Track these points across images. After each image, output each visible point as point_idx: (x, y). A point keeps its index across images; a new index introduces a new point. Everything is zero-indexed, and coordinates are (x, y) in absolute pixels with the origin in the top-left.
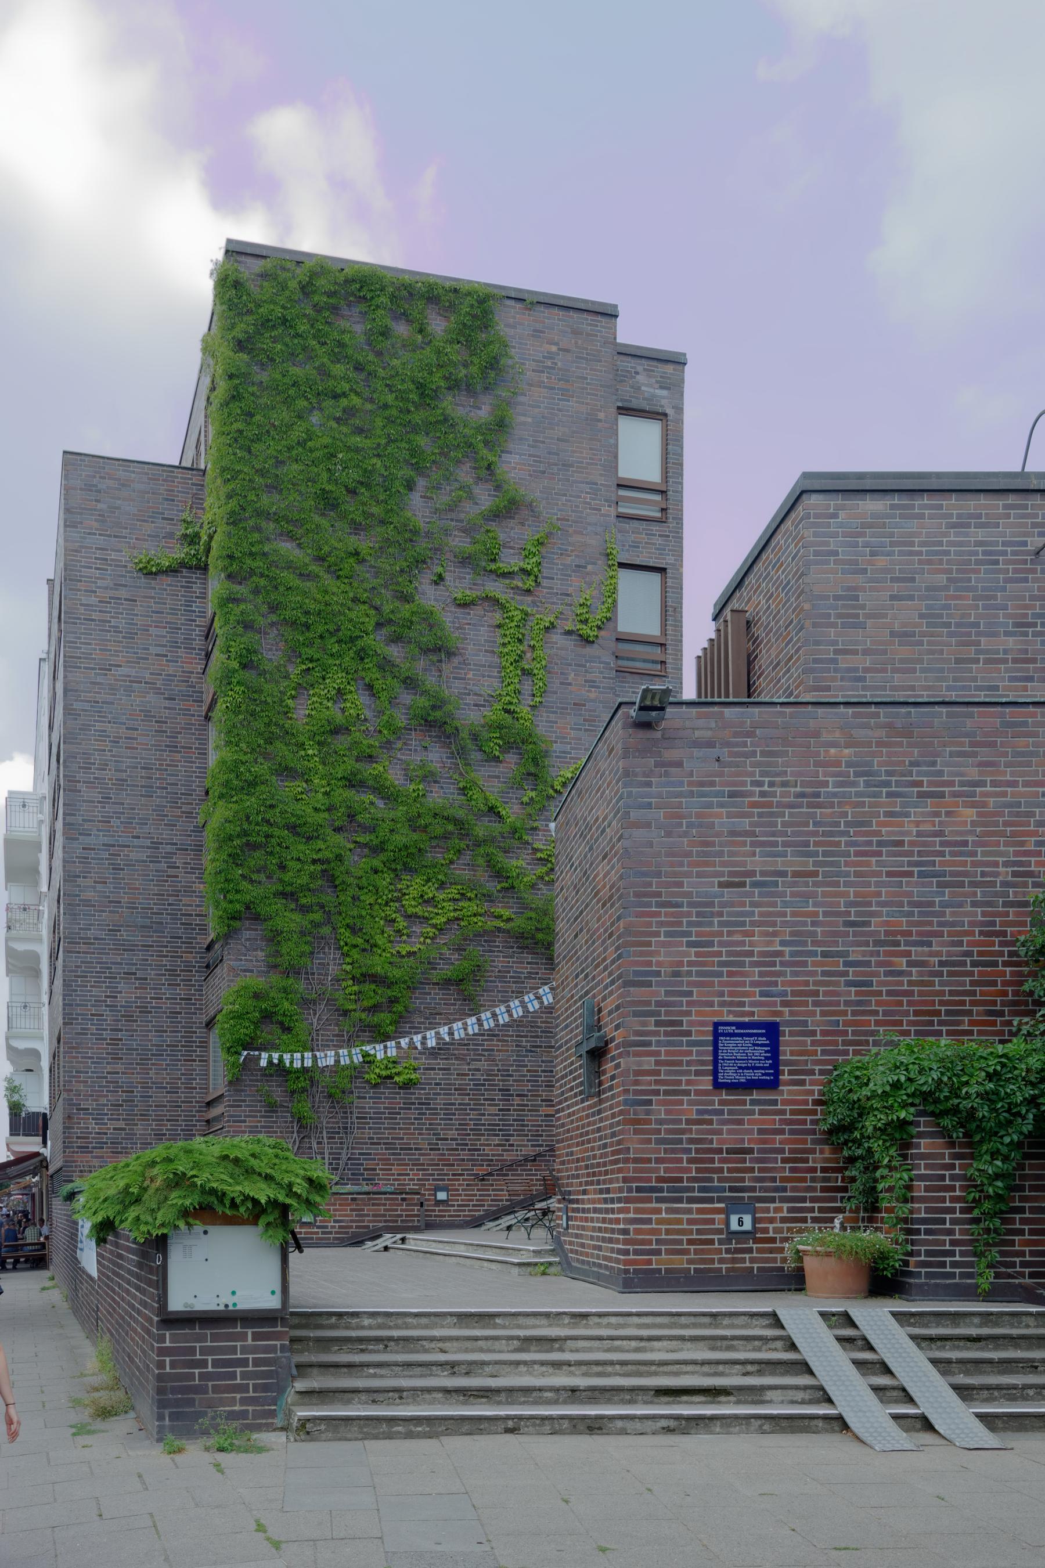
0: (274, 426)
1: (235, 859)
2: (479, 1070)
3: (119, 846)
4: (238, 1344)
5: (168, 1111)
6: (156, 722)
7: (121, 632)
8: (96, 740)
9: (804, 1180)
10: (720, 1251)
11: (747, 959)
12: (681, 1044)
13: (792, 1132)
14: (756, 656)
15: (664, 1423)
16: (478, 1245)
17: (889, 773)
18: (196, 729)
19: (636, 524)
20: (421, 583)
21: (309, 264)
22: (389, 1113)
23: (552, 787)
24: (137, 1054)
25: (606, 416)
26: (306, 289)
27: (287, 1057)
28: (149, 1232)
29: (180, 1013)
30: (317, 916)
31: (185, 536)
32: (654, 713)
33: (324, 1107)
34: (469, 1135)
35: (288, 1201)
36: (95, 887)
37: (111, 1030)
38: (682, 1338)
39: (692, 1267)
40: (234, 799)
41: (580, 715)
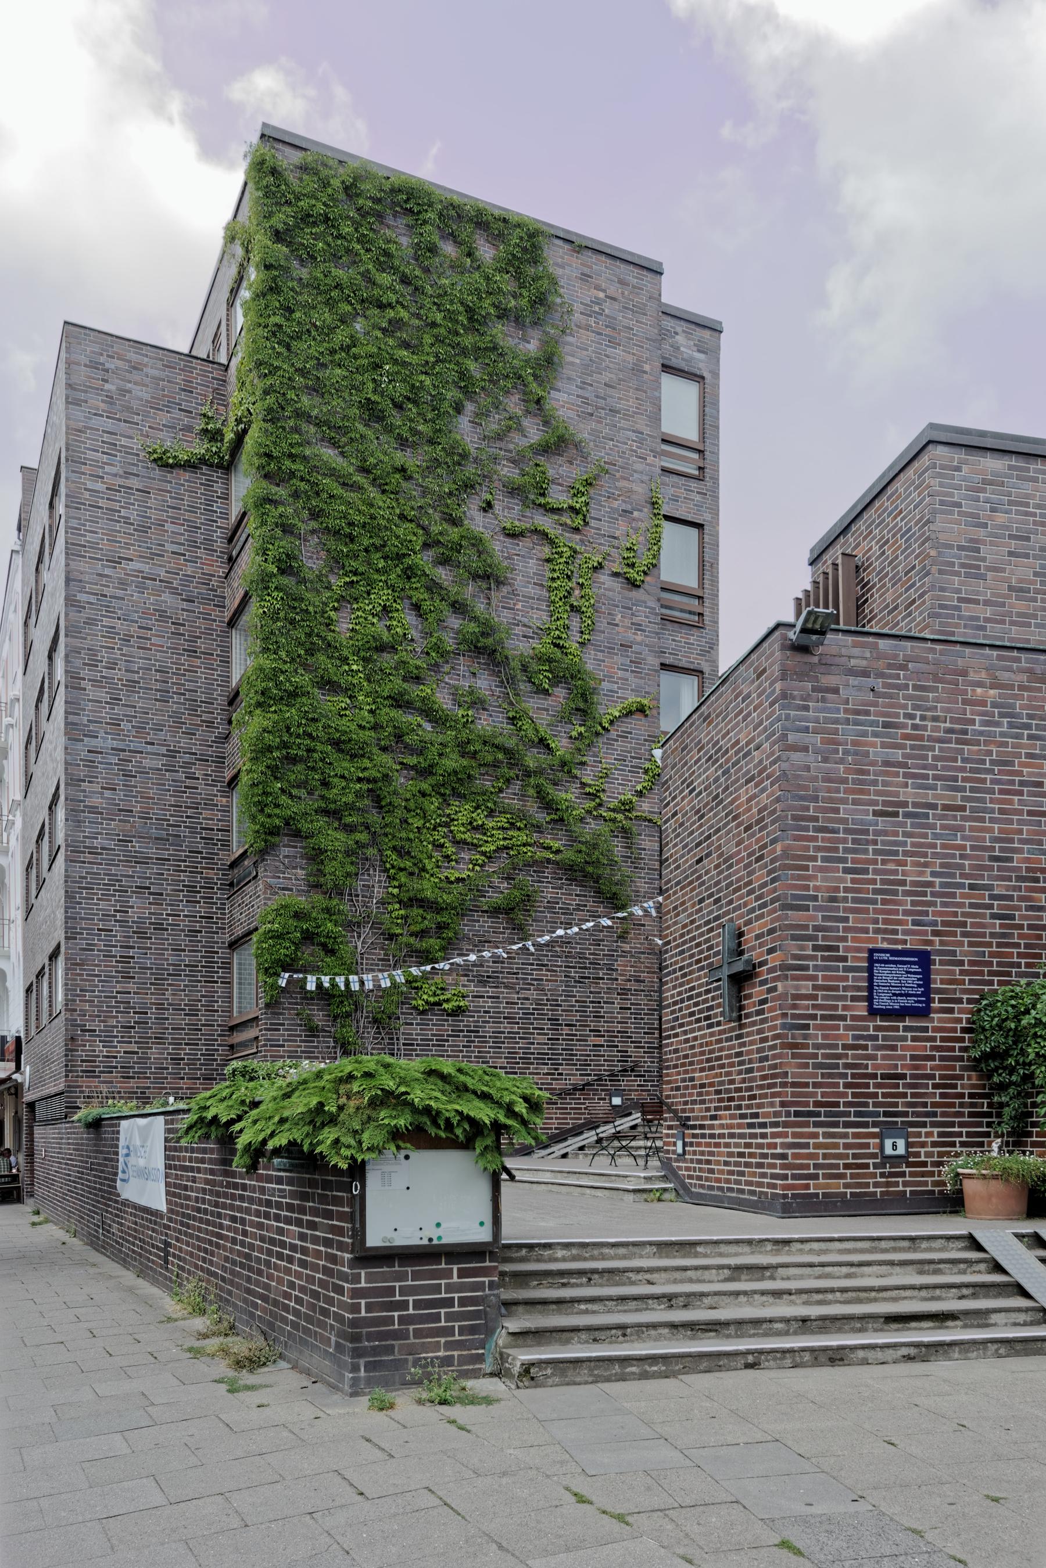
0: (315, 326)
1: (274, 771)
2: (528, 999)
3: (130, 751)
4: (443, 1282)
5: (186, 1034)
6: (173, 623)
7: (133, 524)
8: (103, 636)
9: (953, 1105)
10: (874, 1176)
11: (900, 888)
12: (837, 969)
13: (942, 1058)
14: (866, 600)
15: (905, 1351)
16: (569, 1172)
17: (1030, 717)
18: (217, 635)
19: (675, 479)
20: (469, 509)
21: (353, 164)
22: (437, 1040)
23: (600, 724)
24: (151, 974)
25: (652, 369)
26: (350, 190)
27: (340, 981)
28: (352, 1157)
29: (201, 932)
30: (363, 837)
31: (205, 431)
32: (814, 637)
33: (368, 1033)
34: (518, 1063)
35: (509, 1122)
36: (102, 793)
37: (121, 947)
38: (891, 1263)
39: (849, 1191)
40: (273, 709)
41: (627, 656)
